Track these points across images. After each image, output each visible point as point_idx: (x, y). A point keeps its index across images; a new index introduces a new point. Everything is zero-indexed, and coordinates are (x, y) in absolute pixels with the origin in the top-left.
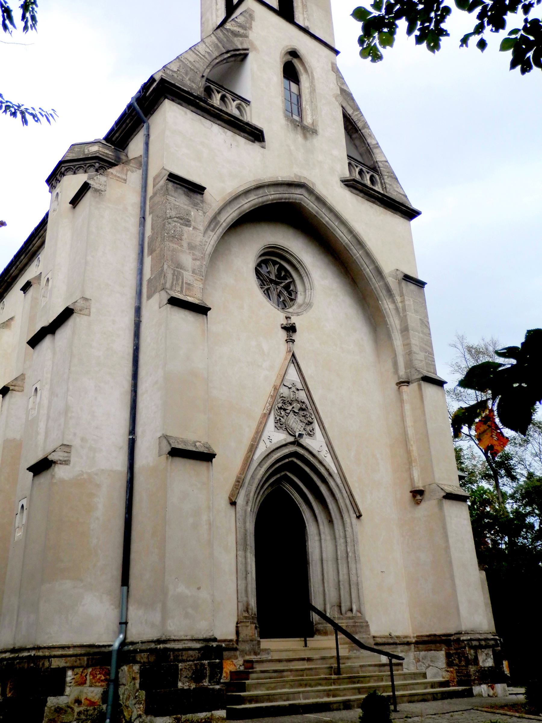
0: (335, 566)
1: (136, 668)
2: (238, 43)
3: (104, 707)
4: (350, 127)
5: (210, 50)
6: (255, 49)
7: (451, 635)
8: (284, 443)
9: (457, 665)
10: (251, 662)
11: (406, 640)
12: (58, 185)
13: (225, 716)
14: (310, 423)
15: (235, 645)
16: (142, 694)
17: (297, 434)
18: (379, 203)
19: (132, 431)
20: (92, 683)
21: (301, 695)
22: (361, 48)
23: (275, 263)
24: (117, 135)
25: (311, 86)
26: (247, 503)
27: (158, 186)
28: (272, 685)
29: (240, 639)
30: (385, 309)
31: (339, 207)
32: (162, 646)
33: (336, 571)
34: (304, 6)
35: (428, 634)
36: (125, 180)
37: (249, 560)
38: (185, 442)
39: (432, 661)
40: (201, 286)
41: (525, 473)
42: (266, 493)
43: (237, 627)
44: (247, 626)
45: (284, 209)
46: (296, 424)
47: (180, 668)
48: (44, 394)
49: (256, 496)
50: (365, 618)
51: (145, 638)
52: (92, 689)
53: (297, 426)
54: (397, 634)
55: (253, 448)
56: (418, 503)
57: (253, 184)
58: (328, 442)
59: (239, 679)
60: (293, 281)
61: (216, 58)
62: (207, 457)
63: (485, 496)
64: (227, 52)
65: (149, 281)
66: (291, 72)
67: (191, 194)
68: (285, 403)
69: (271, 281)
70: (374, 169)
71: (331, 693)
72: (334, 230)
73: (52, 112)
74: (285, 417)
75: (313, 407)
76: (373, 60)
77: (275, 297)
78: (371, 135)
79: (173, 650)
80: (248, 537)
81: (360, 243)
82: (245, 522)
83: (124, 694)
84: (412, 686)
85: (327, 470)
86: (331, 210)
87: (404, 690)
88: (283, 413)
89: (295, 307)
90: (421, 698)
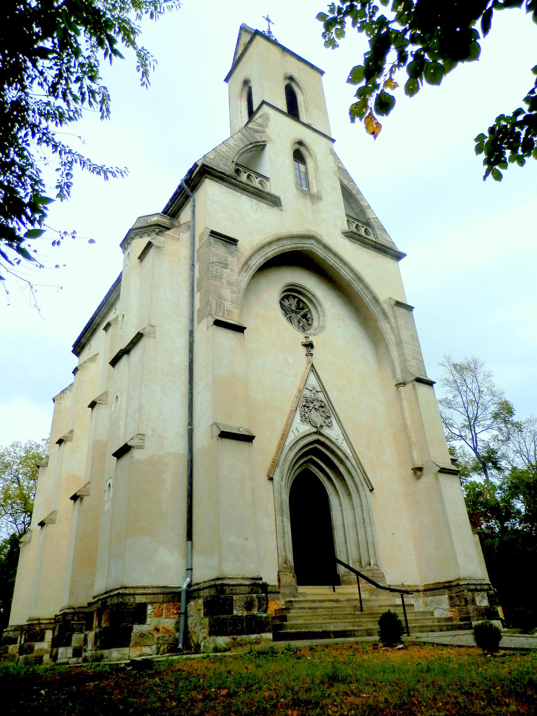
0: (354, 530)
1: (201, 601)
2: (258, 137)
3: (177, 634)
4: (347, 194)
5: (238, 144)
6: (271, 141)
7: (452, 582)
8: (309, 433)
9: (458, 606)
10: (291, 601)
11: (415, 589)
12: (129, 247)
13: (272, 638)
14: (328, 417)
15: (278, 590)
16: (206, 621)
17: (318, 426)
18: (373, 249)
19: (191, 423)
20: (167, 616)
21: (332, 625)
22: (324, 40)
23: (294, 297)
24: (171, 209)
25: (315, 166)
26: (282, 479)
27: (203, 241)
28: (309, 618)
29: (281, 585)
30: (383, 328)
31: (341, 252)
32: (219, 582)
33: (355, 535)
34: (307, 110)
35: (433, 582)
36: (179, 239)
37: (285, 523)
38: (231, 428)
39: (437, 604)
40: (238, 312)
41: (510, 467)
42: (297, 473)
43: (278, 575)
44: (286, 575)
45: (298, 257)
46: (317, 418)
47: (234, 599)
48: (123, 399)
49: (288, 474)
50: (381, 571)
51: (206, 579)
52: (167, 620)
53: (318, 420)
54: (409, 584)
55: (284, 437)
56: (418, 478)
57: (275, 237)
58: (343, 432)
59: (282, 616)
60: (310, 311)
61: (242, 149)
62: (249, 439)
63: (477, 489)
64: (251, 144)
65: (199, 310)
66: (298, 156)
67: (228, 245)
68: (307, 402)
69: (293, 311)
70: (367, 224)
71: (355, 624)
72: (339, 270)
73: (125, 169)
74: (309, 413)
75: (330, 404)
76: (333, 48)
77: (296, 323)
78: (364, 199)
79: (229, 585)
80: (284, 505)
81: (360, 279)
82: (281, 494)
83: (192, 623)
84: (422, 621)
85: (344, 454)
86: (335, 255)
87: (415, 623)
88: (307, 410)
89: (312, 330)
90: (429, 629)
